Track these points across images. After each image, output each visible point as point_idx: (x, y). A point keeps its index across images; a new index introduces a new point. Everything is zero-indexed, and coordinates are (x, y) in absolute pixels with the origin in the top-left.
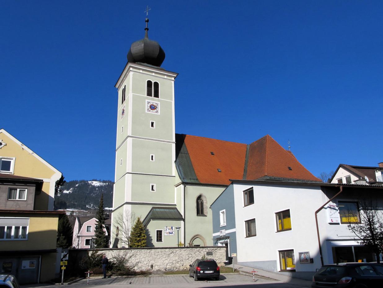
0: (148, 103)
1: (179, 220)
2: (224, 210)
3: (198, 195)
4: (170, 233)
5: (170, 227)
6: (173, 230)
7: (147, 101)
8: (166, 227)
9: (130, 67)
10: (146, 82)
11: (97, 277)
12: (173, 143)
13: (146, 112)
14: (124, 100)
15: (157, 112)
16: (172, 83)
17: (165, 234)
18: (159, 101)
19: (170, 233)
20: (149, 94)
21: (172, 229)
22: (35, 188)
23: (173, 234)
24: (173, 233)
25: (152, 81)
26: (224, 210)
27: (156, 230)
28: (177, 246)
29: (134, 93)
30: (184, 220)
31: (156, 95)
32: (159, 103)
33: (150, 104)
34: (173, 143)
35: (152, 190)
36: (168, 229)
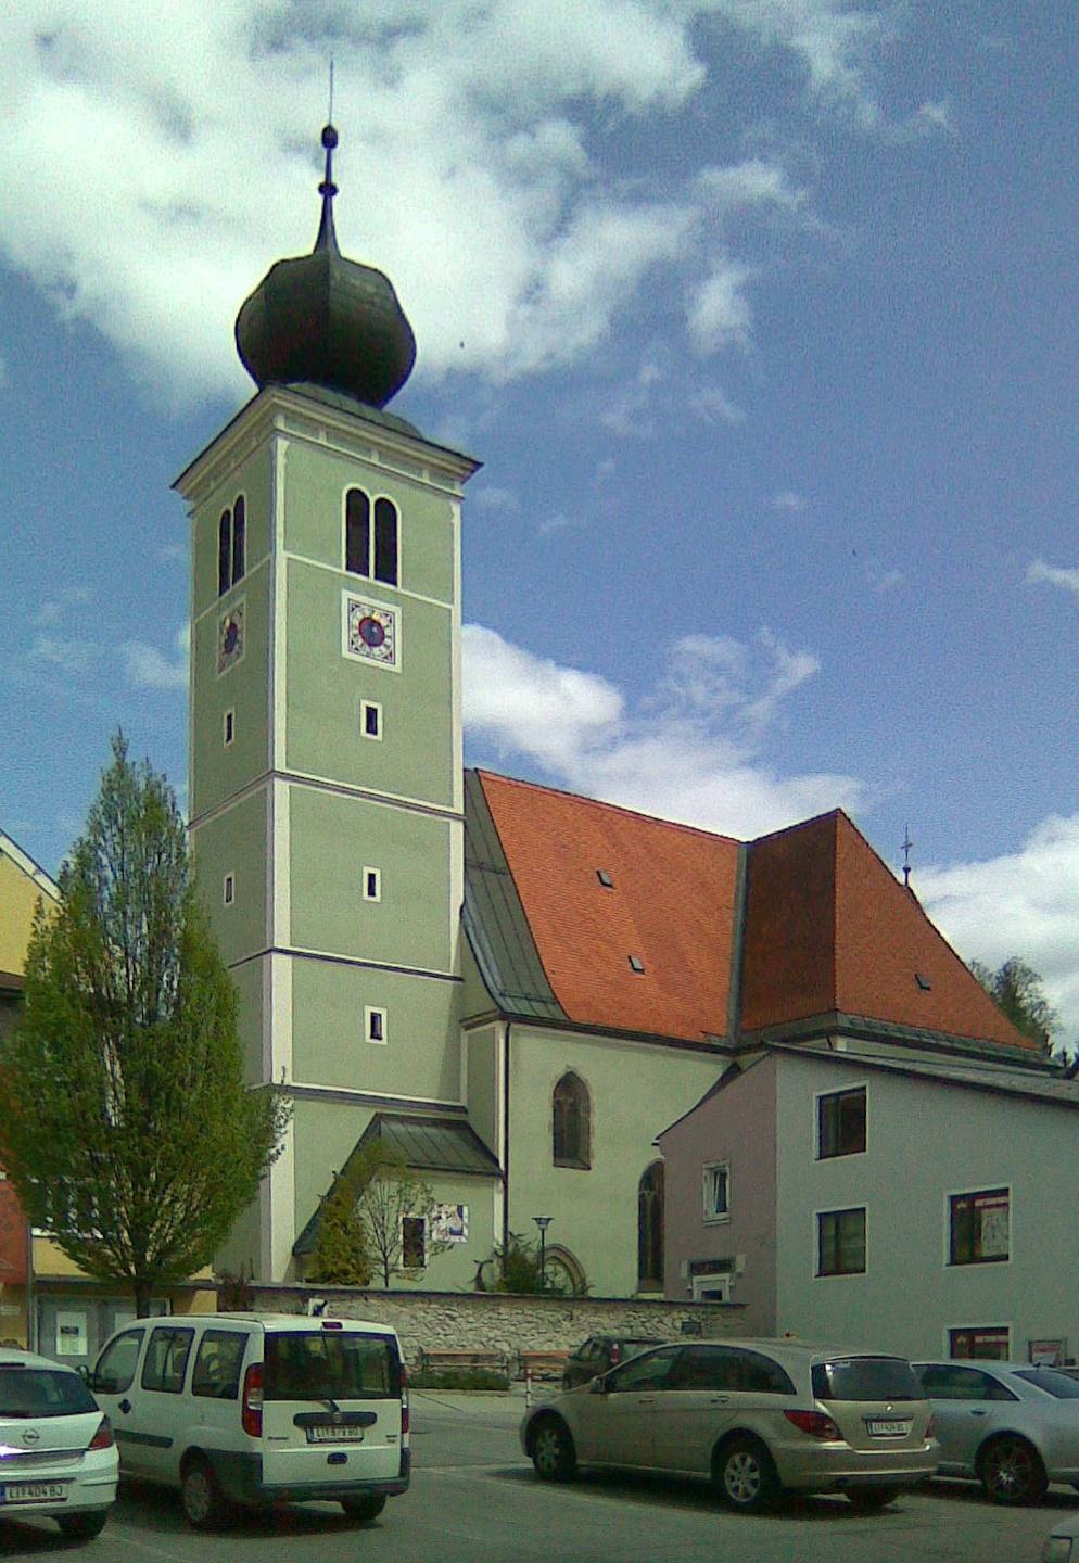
0: (354, 607)
1: (459, 1176)
2: (397, 668)
3: (559, 1071)
4: (452, 1233)
5: (454, 1208)
6: (466, 1220)
7: (346, 595)
8: (440, 1206)
9: (273, 396)
10: (341, 497)
11: (44, 1473)
12: (455, 817)
13: (346, 653)
14: (239, 573)
15: (390, 657)
16: (450, 508)
17: (434, 1234)
18: (397, 599)
19: (452, 1233)
20: (356, 563)
21: (461, 1216)
22: (985, 1243)
23: (464, 1240)
24: (465, 1231)
25: (369, 495)
26: (397, 668)
27: (868, 1152)
28: (471, 1288)
29: (292, 550)
30: (505, 1177)
31: (387, 573)
32: (397, 610)
33: (360, 616)
34: (455, 817)
35: (372, 1037)
36: (444, 1216)
